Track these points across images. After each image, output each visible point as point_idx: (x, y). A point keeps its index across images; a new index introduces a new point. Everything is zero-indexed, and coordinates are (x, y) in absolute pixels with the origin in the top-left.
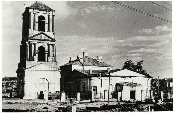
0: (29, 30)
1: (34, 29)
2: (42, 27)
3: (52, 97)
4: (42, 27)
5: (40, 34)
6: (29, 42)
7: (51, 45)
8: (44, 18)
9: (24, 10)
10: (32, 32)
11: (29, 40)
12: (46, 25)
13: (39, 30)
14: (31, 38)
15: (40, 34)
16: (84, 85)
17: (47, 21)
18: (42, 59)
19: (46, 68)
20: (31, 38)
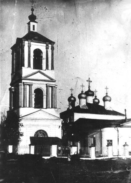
0: (23, 67)
1: (29, 66)
2: (38, 65)
3: (63, 153)
4: (38, 65)
5: (37, 72)
6: (23, 83)
7: (28, 85)
8: (35, 50)
9: (14, 42)
10: (26, 71)
11: (23, 81)
12: (44, 62)
13: (35, 68)
14: (26, 78)
15: (37, 72)
16: (119, 122)
17: (44, 56)
18: (39, 104)
19: (47, 117)
20: (26, 78)
